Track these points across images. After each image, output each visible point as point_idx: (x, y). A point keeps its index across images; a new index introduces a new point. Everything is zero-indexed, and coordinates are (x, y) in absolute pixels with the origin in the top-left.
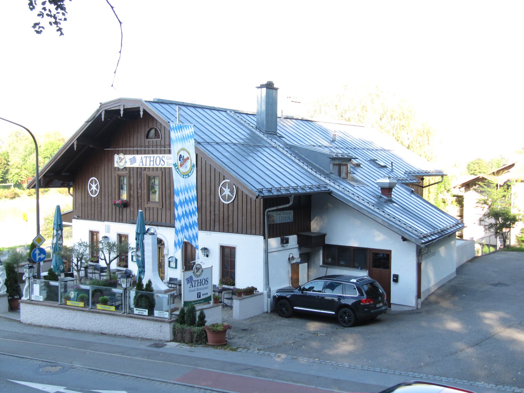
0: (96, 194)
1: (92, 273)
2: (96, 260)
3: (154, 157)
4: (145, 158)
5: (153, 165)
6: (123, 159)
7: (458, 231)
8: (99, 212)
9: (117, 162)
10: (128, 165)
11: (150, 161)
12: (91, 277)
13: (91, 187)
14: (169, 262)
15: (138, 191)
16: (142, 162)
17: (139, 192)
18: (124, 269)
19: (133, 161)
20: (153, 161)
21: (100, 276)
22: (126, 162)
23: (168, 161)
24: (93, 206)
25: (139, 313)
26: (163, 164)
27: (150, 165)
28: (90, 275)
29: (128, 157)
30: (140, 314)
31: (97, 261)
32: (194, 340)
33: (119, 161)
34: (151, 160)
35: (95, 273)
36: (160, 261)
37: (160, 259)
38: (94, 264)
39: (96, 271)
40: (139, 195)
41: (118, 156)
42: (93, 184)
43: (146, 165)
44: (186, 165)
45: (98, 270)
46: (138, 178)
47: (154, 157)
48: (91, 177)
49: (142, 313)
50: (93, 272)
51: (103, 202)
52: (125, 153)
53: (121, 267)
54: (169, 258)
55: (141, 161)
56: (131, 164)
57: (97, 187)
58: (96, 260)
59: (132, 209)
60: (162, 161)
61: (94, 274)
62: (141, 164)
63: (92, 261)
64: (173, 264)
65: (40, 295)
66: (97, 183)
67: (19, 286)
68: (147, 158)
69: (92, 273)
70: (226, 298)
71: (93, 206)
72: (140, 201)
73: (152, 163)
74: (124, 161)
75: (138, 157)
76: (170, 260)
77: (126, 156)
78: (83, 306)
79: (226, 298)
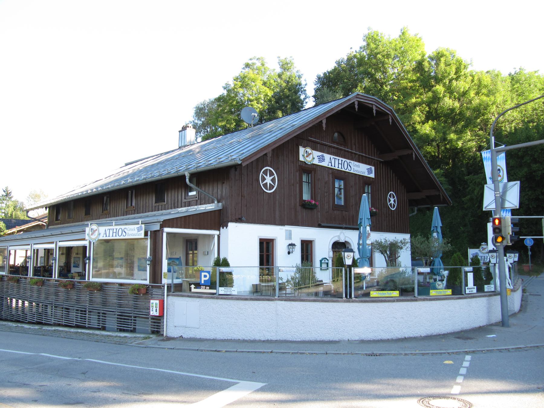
3: (342, 161)
4: (334, 159)
5: (342, 168)
6: (311, 154)
7: (188, 271)
9: (303, 156)
10: (316, 162)
11: (113, 233)
16: (331, 163)
19: (322, 159)
20: (116, 232)
22: (314, 158)
23: (354, 167)
25: (469, 291)
26: (350, 169)
27: (338, 167)
29: (316, 154)
30: (470, 293)
32: (85, 313)
34: (114, 232)
42: (267, 176)
43: (335, 166)
49: (472, 291)
52: (99, 225)
55: (105, 233)
60: (123, 233)
62: (330, 164)
65: (474, 285)
68: (111, 230)
73: (114, 234)
75: (327, 157)
78: (451, 294)
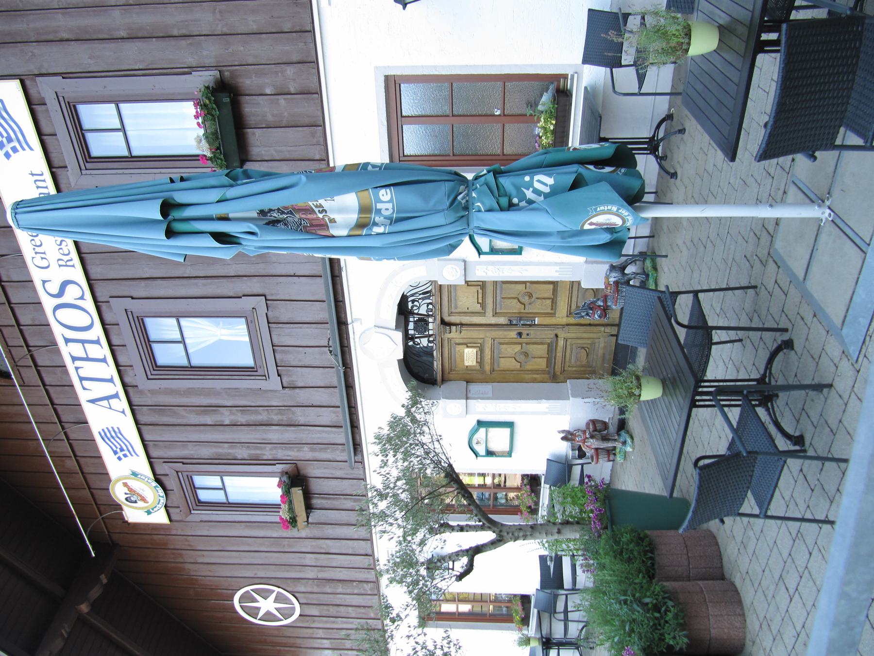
0: (290, 600)
1: (566, 620)
2: (519, 603)
6: (125, 485)
8: (349, 591)
9: (149, 513)
12: (581, 625)
13: (269, 616)
14: (490, 453)
15: (227, 422)
17: (233, 417)
18: (545, 491)
19: (122, 452)
21: (574, 589)
24: (333, 611)
28: (574, 630)
29: (115, 467)
31: (523, 604)
33: (140, 504)
35: (566, 612)
36: (502, 320)
37: (493, 321)
38: (534, 612)
39: (560, 606)
40: (242, 419)
41: (124, 507)
44: (139, 489)
45: (556, 597)
46: (180, 421)
47: (67, 341)
48: (237, 612)
50: (562, 616)
51: (310, 574)
53: (537, 503)
54: (476, 454)
55: (105, 403)
56: (132, 452)
57: (265, 594)
58: (518, 607)
59: (310, 455)
61: (571, 616)
63: (525, 621)
64: (498, 439)
66: (247, 592)
67: (712, 540)
69: (566, 620)
70: (640, 88)
71: (333, 611)
72: (263, 417)
74: (135, 484)
76: (481, 450)
77: (113, 475)
79: (640, 88)
